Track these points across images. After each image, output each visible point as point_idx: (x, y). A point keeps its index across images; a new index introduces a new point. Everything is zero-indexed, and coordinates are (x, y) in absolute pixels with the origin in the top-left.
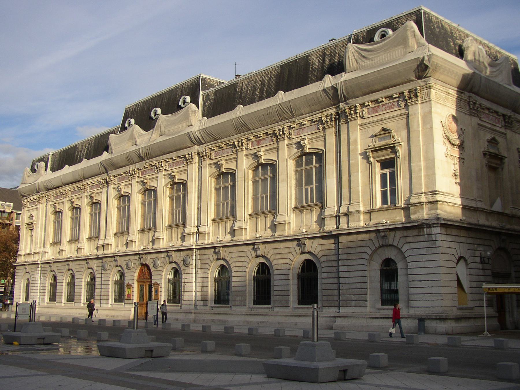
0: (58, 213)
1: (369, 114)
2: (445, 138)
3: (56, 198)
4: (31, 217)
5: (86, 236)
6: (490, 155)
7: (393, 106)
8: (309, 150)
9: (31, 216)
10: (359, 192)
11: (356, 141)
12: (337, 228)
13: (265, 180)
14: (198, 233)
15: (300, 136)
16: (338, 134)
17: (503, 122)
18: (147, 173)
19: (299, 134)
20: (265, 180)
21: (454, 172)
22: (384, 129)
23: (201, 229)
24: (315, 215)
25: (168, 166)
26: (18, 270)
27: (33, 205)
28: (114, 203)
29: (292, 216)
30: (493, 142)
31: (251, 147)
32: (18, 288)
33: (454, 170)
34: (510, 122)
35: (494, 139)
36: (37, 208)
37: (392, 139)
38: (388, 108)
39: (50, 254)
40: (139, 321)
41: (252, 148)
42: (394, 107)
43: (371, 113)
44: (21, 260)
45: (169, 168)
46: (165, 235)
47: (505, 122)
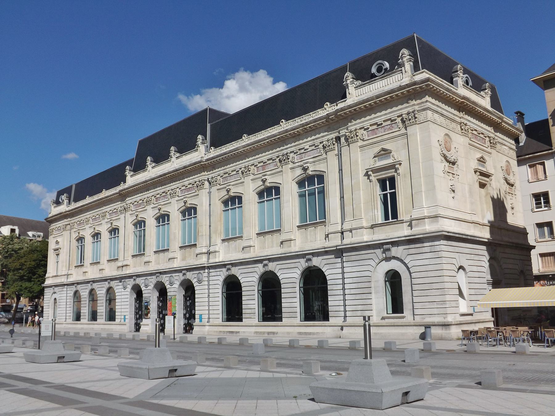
0: (81, 239)
1: (368, 136)
2: (442, 156)
3: (79, 226)
4: (57, 242)
5: (153, 250)
6: (480, 172)
7: (392, 127)
8: (312, 172)
9: (57, 242)
10: (361, 208)
11: (357, 161)
12: (208, 261)
13: (312, 194)
14: (209, 253)
15: (302, 160)
16: (340, 156)
17: (489, 142)
18: (161, 199)
19: (302, 158)
20: (312, 194)
21: (503, 177)
22: (383, 150)
23: (212, 249)
24: (319, 232)
25: (180, 193)
26: (46, 291)
27: (59, 232)
28: (131, 228)
29: (297, 233)
30: (482, 160)
31: (257, 172)
32: (47, 307)
33: (451, 186)
34: (494, 142)
35: (482, 157)
36: (62, 235)
37: (392, 158)
38: (387, 130)
39: (76, 276)
40: (51, 335)
41: (258, 173)
42: (393, 129)
43: (370, 135)
44: (48, 282)
45: (181, 194)
46: (256, 242)
47: (491, 143)
